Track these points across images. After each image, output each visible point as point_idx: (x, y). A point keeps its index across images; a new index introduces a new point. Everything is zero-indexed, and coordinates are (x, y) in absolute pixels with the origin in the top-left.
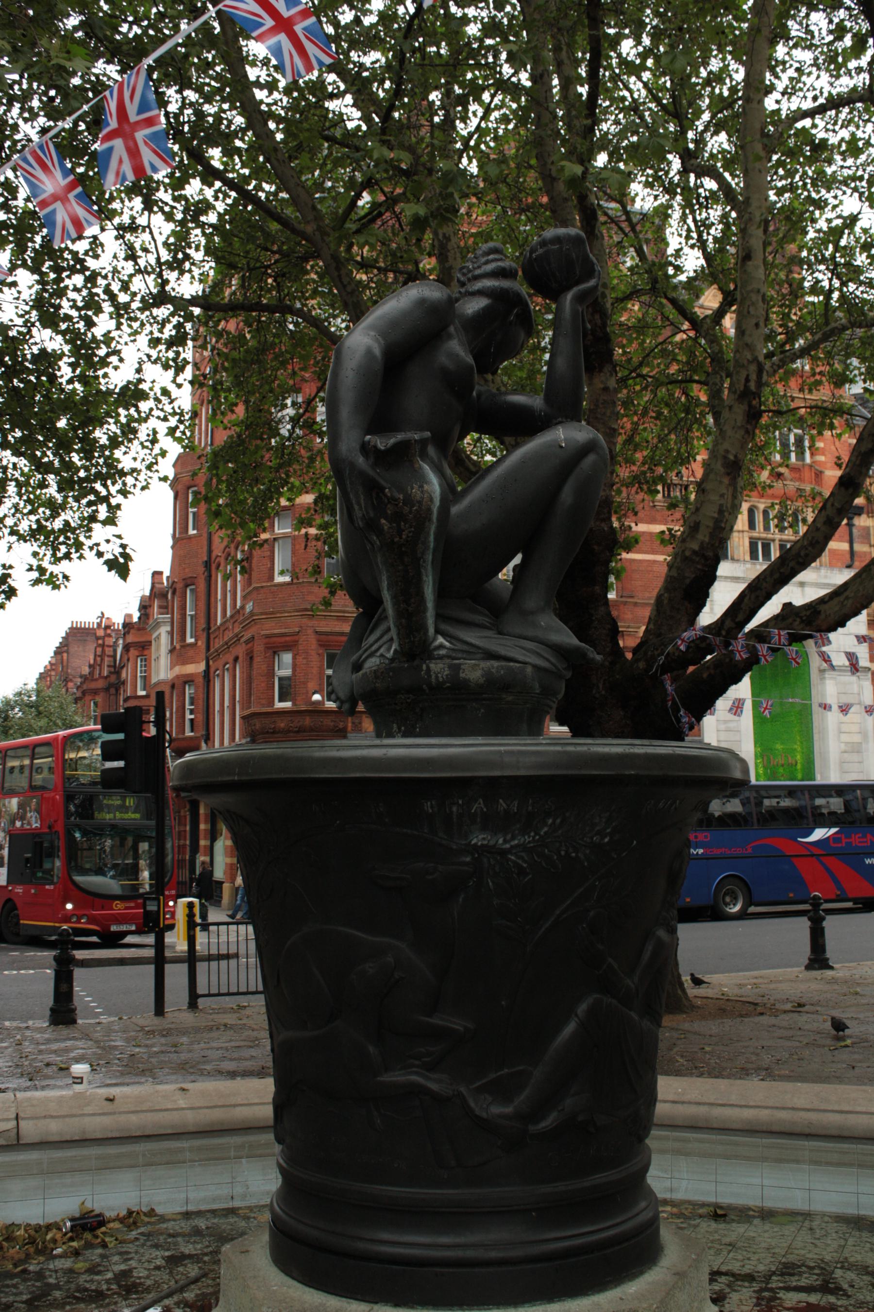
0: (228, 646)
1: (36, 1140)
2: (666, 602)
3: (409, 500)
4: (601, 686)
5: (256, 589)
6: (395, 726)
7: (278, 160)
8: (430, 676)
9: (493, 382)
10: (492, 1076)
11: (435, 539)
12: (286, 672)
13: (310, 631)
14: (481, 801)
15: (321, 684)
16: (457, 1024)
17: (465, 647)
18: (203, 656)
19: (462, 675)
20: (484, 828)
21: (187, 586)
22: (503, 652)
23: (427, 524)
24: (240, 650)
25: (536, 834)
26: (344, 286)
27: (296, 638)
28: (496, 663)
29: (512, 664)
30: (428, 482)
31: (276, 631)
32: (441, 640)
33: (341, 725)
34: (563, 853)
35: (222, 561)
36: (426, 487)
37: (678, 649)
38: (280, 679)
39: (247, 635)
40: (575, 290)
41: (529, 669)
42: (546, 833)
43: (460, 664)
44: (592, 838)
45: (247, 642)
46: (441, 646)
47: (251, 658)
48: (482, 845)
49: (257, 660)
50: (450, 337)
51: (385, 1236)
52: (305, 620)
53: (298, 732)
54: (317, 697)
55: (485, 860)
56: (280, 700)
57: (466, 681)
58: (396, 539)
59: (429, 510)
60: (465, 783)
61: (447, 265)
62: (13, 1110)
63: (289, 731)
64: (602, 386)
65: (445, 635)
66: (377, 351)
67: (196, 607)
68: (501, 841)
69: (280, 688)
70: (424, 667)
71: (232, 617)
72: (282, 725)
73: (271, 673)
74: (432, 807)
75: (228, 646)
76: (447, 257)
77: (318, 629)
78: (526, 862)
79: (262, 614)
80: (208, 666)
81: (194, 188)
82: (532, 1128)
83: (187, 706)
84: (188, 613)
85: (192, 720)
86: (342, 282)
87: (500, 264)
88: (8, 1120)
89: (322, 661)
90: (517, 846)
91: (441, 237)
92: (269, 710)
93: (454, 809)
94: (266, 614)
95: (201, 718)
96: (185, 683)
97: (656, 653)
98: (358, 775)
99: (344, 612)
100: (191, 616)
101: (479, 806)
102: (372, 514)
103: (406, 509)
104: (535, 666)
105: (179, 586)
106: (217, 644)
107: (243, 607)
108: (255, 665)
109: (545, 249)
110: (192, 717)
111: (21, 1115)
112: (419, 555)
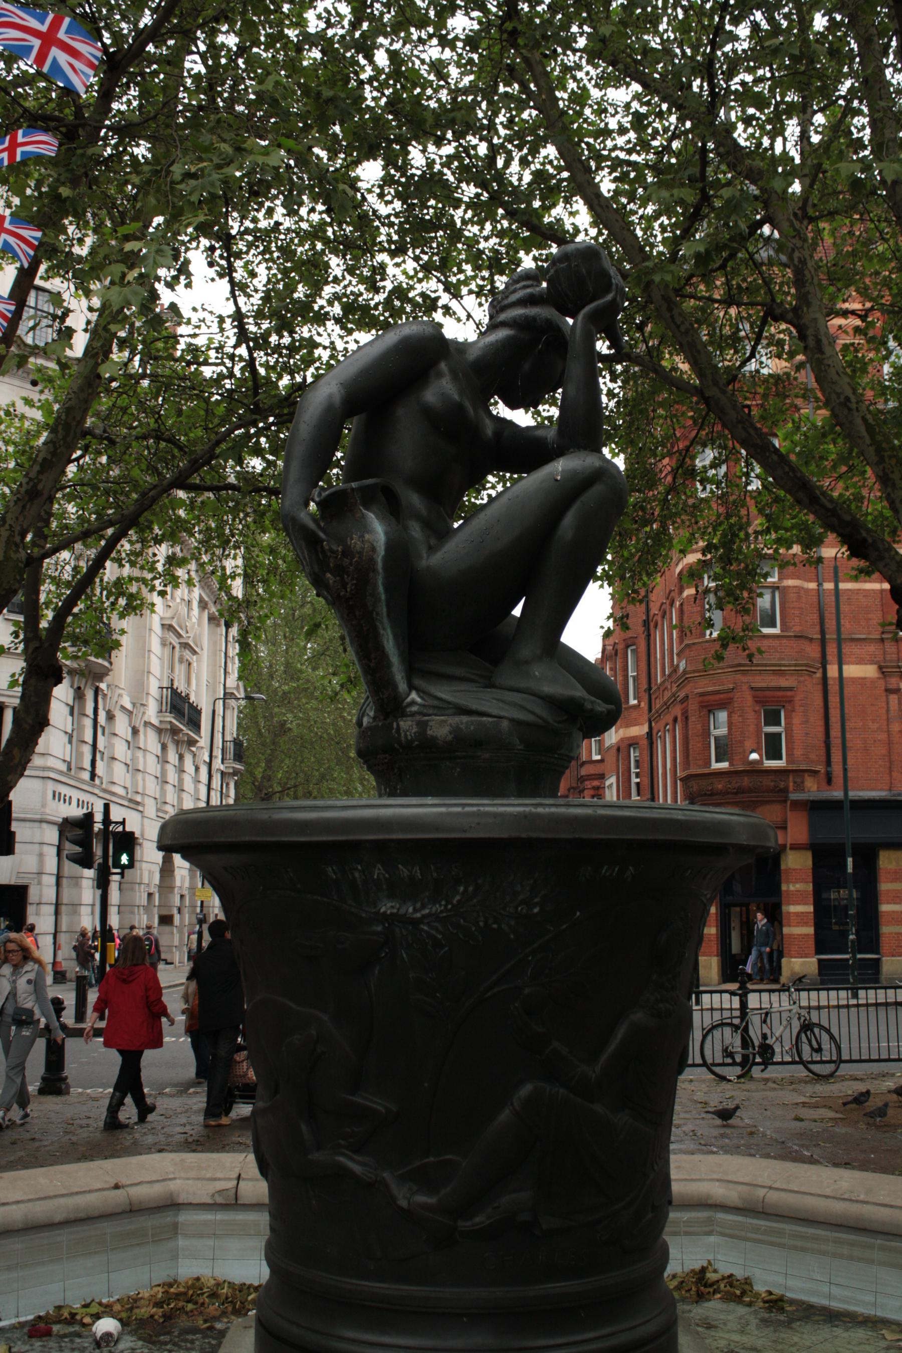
0: (667, 706)
1: (254, 1201)
3: (347, 552)
5: (688, 646)
7: (601, 207)
8: (399, 734)
9: (858, 410)
11: (386, 590)
12: (723, 731)
13: (745, 687)
14: (379, 866)
15: (759, 743)
16: (379, 1105)
17: (436, 703)
18: (646, 717)
19: (429, 732)
20: (391, 896)
21: (627, 647)
22: (474, 707)
23: (371, 575)
24: (677, 711)
25: (447, 903)
26: (678, 327)
27: (731, 695)
28: (465, 719)
29: (485, 719)
31: (711, 689)
32: (414, 695)
33: (782, 785)
34: (481, 924)
35: (659, 618)
36: (367, 536)
38: (716, 738)
39: (682, 695)
40: (587, 309)
41: (505, 724)
42: (459, 901)
44: (516, 908)
45: (682, 702)
46: (413, 703)
47: (687, 718)
48: (392, 914)
49: (692, 719)
50: (440, 375)
52: (738, 676)
53: (736, 793)
54: (754, 756)
56: (717, 761)
57: (434, 738)
59: (372, 561)
60: (355, 847)
62: (237, 1171)
63: (727, 793)
65: (418, 691)
66: (337, 400)
67: (637, 668)
68: (411, 910)
69: (716, 748)
70: (395, 725)
71: (669, 676)
72: (720, 786)
73: (707, 734)
74: (335, 873)
75: (667, 706)
77: (753, 685)
79: (694, 671)
80: (650, 727)
82: (463, 1225)
83: (633, 770)
84: (630, 674)
85: (638, 784)
86: (675, 323)
87: (529, 290)
88: (230, 1179)
89: (759, 718)
90: (429, 915)
91: (796, 262)
92: (706, 771)
93: (357, 875)
94: (699, 671)
95: (646, 781)
96: (630, 745)
99: (780, 665)
100: (634, 677)
103: (346, 561)
104: (512, 720)
105: (620, 647)
106: (657, 704)
107: (678, 666)
108: (690, 726)
110: (638, 780)
111: (243, 1176)
112: (371, 608)
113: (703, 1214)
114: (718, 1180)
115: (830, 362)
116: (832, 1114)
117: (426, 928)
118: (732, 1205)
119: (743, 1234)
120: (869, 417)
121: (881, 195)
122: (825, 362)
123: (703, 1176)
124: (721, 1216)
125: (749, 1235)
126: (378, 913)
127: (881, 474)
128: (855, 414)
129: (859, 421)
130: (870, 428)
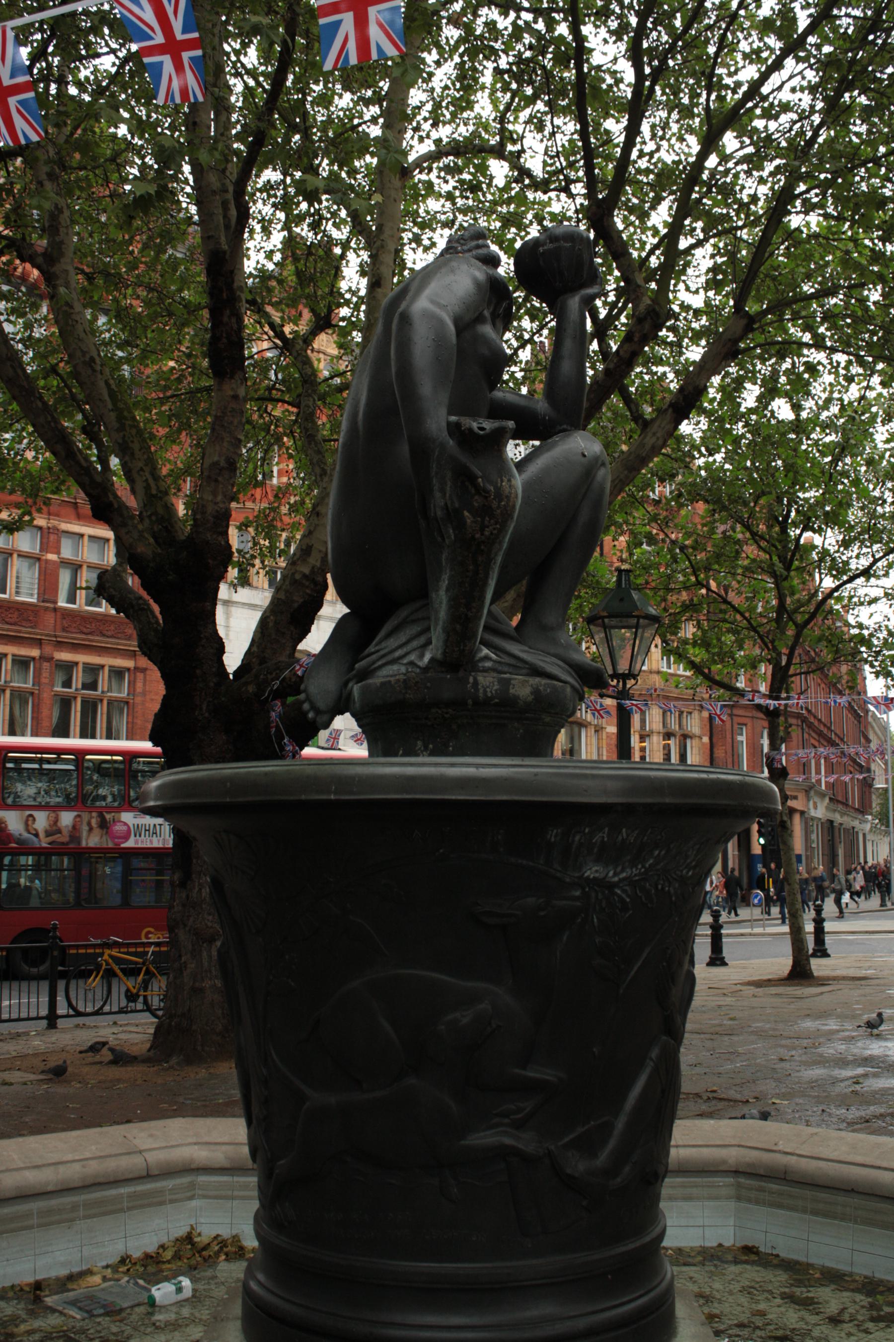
2: (271, 624)
4: (204, 707)
6: (419, 743)
8: (477, 690)
10: (580, 1130)
19: (512, 691)
25: (643, 867)
28: (544, 681)
30: (514, 477)
32: (485, 651)
37: (295, 674)
43: (510, 679)
46: (487, 658)
51: (399, 1318)
55: (593, 895)
57: (516, 698)
58: (477, 536)
61: (57, 239)
64: (232, 393)
68: (611, 873)
70: (471, 680)
76: (58, 230)
78: (628, 896)
81: (664, 98)
90: (624, 879)
97: (269, 677)
98: (505, 798)
101: (602, 836)
102: (457, 505)
103: (495, 504)
109: (556, 245)
113: (185, 1180)
114: (195, 1144)
115: (78, 318)
116: (32, 1077)
117: (619, 892)
118: (217, 1166)
119: (230, 1193)
120: (112, 382)
121: (872, 271)
122: (74, 317)
123: (180, 1142)
124: (203, 1179)
125: (236, 1193)
126: (581, 877)
127: (120, 441)
128: (100, 376)
129: (102, 384)
130: (112, 394)
